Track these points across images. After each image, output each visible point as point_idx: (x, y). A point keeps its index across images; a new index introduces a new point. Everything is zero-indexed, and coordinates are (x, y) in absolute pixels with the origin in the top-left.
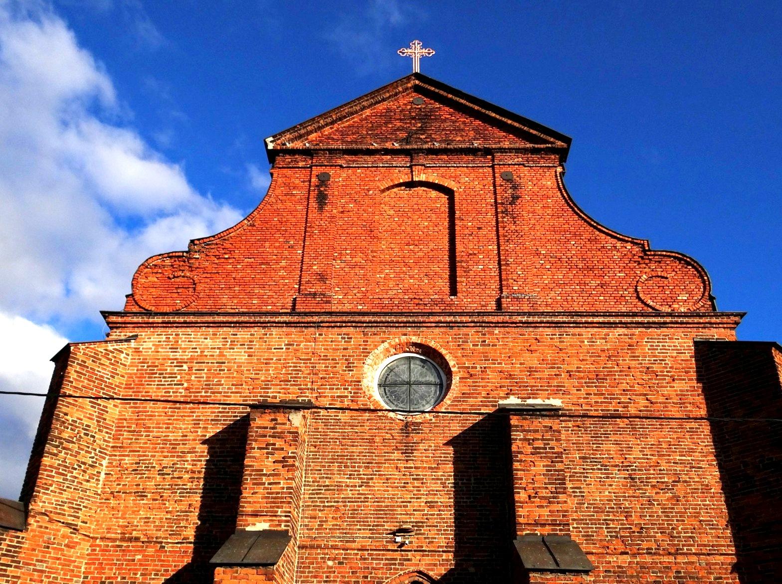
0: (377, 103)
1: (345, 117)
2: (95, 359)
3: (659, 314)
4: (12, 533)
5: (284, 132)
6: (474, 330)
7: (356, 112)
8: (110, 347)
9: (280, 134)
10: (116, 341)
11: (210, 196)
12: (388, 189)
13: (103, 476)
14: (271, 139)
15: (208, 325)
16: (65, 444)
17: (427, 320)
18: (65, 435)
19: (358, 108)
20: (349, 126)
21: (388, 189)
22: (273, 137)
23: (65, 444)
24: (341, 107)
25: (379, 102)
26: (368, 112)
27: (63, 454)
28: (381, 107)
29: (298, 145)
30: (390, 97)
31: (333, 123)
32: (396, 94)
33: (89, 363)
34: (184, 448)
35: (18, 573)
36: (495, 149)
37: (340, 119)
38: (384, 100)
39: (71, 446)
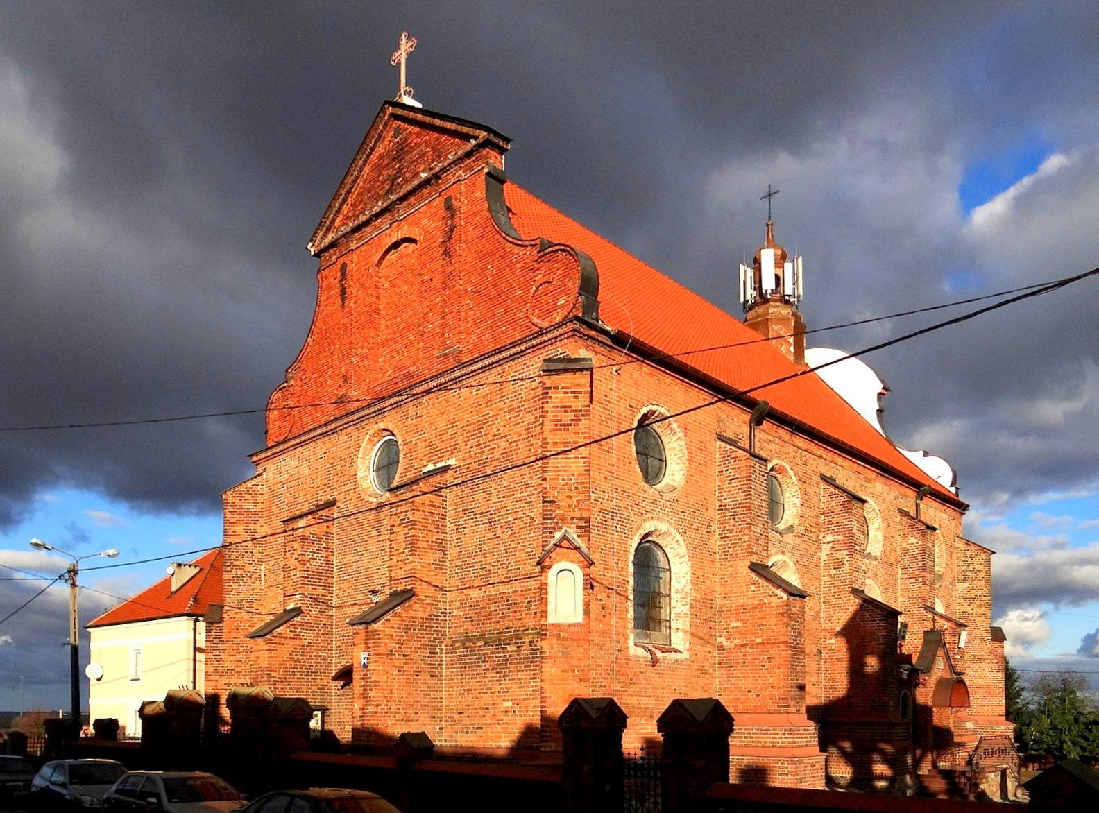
0: (368, 157)
1: (351, 188)
2: (241, 498)
3: (543, 332)
4: (216, 625)
5: (316, 233)
6: (412, 403)
7: (357, 178)
8: (249, 484)
9: (314, 236)
10: (252, 479)
11: (19, 518)
12: (382, 258)
13: (263, 577)
14: (310, 244)
15: (295, 446)
16: (235, 563)
17: (385, 406)
18: (233, 557)
19: (355, 173)
20: (359, 194)
21: (382, 258)
22: (311, 241)
23: (235, 563)
24: (344, 179)
25: (370, 154)
26: (367, 169)
27: (234, 570)
28: (374, 157)
29: (330, 237)
30: (376, 142)
31: (345, 200)
32: (380, 136)
33: (237, 503)
34: (554, 463)
35: (224, 647)
36: (439, 172)
37: (348, 192)
38: (372, 149)
39: (238, 563)
